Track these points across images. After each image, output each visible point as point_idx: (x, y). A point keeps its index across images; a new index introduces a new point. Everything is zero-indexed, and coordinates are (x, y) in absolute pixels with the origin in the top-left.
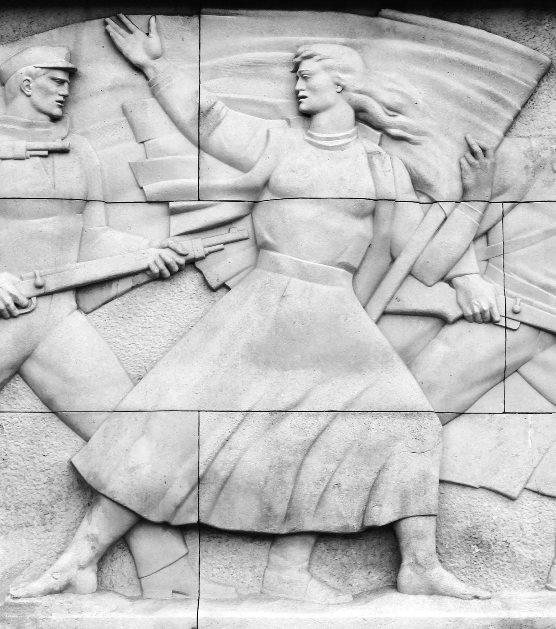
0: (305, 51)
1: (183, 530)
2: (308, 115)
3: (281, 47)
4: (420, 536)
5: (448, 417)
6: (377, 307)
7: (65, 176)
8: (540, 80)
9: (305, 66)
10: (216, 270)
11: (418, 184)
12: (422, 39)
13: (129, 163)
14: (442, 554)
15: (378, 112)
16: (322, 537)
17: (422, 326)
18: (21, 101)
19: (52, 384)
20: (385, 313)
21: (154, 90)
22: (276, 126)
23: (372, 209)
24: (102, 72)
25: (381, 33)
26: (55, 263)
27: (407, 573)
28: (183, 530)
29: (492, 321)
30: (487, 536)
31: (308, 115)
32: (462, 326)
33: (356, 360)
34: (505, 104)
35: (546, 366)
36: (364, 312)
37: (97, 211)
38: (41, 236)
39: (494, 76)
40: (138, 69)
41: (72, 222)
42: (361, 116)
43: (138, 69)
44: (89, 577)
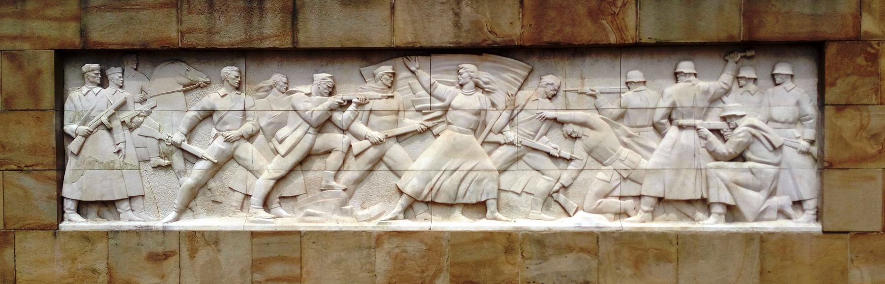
0: (461, 66)
1: (427, 203)
2: (462, 86)
3: (453, 65)
4: (492, 204)
5: (502, 171)
7: (393, 104)
8: (529, 73)
9: (461, 71)
11: (493, 105)
12: (495, 62)
14: (498, 209)
16: (466, 205)
19: (390, 163)
21: (417, 78)
23: (478, 113)
24: (403, 74)
25: (483, 61)
26: (631, 83)
27: (488, 214)
28: (427, 203)
30: (512, 204)
32: (505, 146)
33: (473, 155)
34: (82, 207)
37: (401, 113)
38: (387, 121)
40: (413, 72)
41: (394, 117)
42: (477, 86)
43: (413, 72)
44: (402, 216)
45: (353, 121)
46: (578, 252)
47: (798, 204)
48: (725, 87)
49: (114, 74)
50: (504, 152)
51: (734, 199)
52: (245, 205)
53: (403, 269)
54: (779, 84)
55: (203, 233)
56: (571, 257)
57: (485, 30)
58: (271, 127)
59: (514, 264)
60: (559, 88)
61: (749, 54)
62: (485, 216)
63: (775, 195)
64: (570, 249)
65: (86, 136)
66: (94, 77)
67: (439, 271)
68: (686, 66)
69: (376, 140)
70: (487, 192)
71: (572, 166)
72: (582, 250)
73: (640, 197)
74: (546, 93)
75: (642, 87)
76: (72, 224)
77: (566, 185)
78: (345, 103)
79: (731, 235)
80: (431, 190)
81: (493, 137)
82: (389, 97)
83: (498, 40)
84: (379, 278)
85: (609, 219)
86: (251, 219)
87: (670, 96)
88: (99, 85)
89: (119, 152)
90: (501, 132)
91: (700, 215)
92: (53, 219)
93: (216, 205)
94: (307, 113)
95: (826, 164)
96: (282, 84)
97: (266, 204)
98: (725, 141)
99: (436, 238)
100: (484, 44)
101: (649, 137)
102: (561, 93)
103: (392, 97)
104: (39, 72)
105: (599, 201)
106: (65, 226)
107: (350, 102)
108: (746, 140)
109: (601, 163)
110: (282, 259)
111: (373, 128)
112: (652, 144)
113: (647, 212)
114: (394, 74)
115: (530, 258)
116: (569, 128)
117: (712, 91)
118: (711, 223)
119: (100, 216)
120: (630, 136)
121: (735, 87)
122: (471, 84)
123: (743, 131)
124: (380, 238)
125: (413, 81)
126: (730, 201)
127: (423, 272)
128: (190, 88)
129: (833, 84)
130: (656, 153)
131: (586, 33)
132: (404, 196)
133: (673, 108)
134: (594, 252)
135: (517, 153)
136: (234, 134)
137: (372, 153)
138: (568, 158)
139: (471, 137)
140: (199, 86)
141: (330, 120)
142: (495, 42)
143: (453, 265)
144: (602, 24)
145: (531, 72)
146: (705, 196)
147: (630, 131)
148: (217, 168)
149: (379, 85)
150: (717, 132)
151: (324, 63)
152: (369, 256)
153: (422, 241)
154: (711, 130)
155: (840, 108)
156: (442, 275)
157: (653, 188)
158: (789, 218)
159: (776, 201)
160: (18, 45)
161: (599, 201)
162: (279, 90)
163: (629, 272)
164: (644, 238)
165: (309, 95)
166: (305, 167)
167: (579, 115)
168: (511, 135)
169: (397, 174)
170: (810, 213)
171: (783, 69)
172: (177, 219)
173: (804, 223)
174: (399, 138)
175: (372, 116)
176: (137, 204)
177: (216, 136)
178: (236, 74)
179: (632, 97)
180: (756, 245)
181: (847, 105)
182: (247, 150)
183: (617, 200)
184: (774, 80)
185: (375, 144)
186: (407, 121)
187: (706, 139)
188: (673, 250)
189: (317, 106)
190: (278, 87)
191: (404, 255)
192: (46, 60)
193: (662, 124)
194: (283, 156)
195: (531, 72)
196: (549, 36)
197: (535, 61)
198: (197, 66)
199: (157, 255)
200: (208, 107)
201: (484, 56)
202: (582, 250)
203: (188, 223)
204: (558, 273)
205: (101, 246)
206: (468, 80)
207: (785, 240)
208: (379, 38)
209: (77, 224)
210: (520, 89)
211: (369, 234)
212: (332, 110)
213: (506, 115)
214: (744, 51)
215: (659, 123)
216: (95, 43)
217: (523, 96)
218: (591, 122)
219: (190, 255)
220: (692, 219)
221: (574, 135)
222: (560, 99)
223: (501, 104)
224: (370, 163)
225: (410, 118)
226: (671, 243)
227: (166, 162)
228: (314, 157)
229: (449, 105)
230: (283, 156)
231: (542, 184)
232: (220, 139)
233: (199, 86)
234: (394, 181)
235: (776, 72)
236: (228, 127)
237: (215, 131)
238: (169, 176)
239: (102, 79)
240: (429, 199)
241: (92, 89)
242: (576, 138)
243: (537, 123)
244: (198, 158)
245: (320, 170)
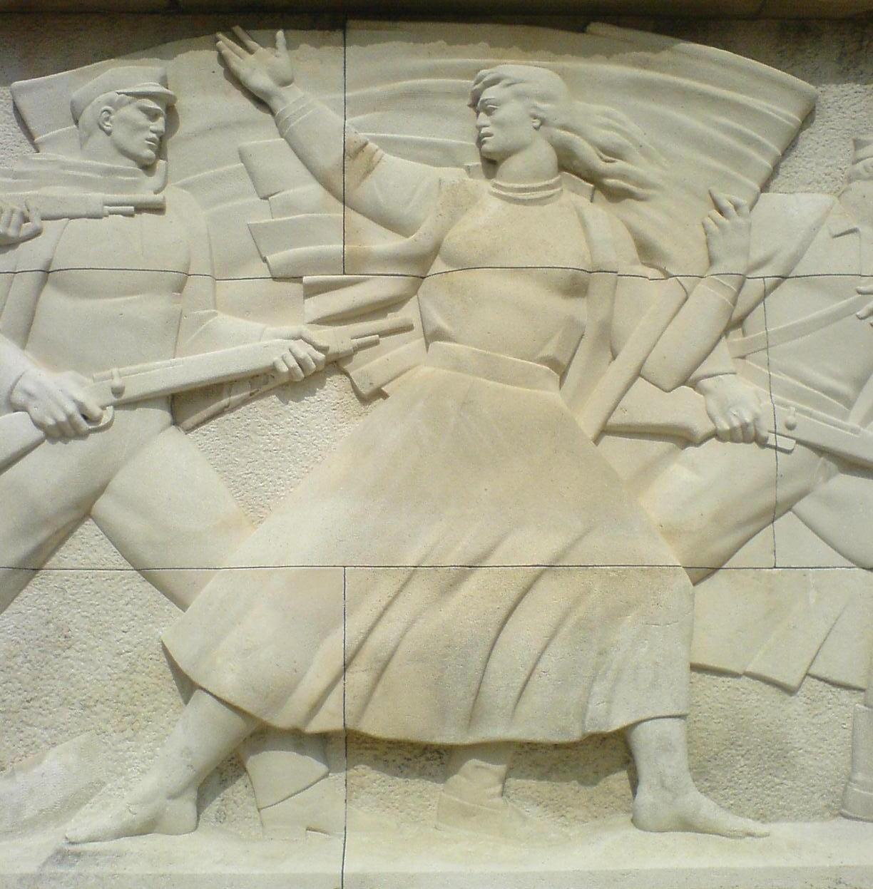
2: (491, 164)
4: (666, 747)
5: (702, 573)
11: (646, 251)
17: (657, 447)
23: (576, 287)
27: (646, 795)
40: (261, 101)
41: (152, 307)
42: (567, 162)
44: (186, 807)
50: (692, 484)
63: (617, 355)
82: (141, 208)
90: (689, 380)
103: (158, 209)
111: (54, 356)
122: (542, 154)
125: (262, 139)
132: (202, 703)
135: (776, 481)
169: (161, 579)
174: (184, 404)
185: (61, 432)
186: (226, 322)
206: (525, 131)
210: (765, 187)
213: (708, 301)
220: (780, 375)
223: (684, 248)
225: (245, 310)
229: (436, 250)
240: (326, 721)
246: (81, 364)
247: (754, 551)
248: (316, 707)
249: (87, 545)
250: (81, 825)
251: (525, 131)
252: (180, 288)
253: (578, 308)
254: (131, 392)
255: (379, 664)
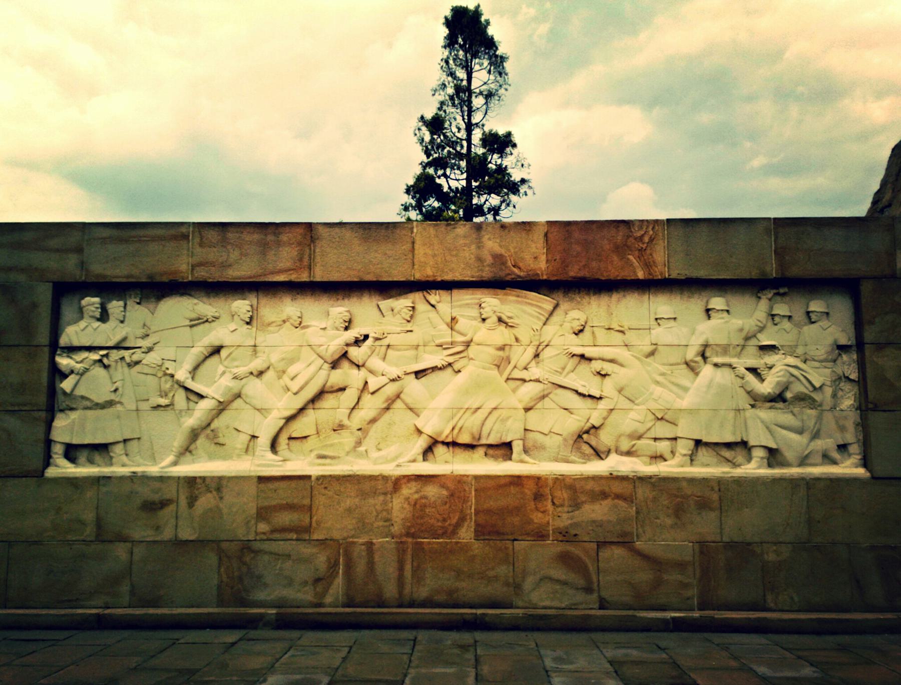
0: (483, 300)
2: (484, 320)
3: (476, 299)
5: (527, 410)
6: (505, 376)
7: (412, 339)
10: (457, 366)
11: (517, 340)
12: (518, 296)
13: (257, 437)
15: (504, 318)
16: (490, 446)
17: (519, 383)
18: (398, 316)
19: (409, 400)
20: (508, 379)
22: (475, 323)
23: (502, 348)
25: (506, 294)
29: (539, 381)
31: (484, 320)
32: (531, 383)
34: (72, 452)
35: (556, 394)
36: (463, 372)
37: (421, 348)
39: (540, 307)
40: (433, 306)
41: (412, 353)
42: (500, 320)
43: (433, 306)
44: (421, 457)
45: (369, 356)
46: (613, 499)
47: (843, 448)
48: (760, 324)
49: (115, 306)
50: (529, 391)
51: (777, 444)
52: (250, 449)
53: (422, 518)
54: (813, 323)
55: (204, 479)
56: (607, 503)
57: (509, 264)
58: (282, 363)
59: (543, 512)
60: (586, 323)
61: (782, 291)
62: (510, 459)
64: (604, 495)
65: (82, 374)
66: (94, 311)
67: (462, 519)
68: (717, 302)
69: (394, 376)
70: (511, 432)
71: (603, 405)
72: (618, 497)
73: (675, 439)
74: (572, 328)
75: (672, 323)
76: (60, 470)
77: (597, 425)
78: (362, 338)
79: (776, 481)
80: (453, 429)
81: (517, 374)
83: (522, 274)
84: (396, 528)
85: (645, 463)
86: (257, 462)
87: (702, 333)
88: (98, 320)
89: (116, 390)
90: (526, 368)
91: (740, 459)
92: (37, 463)
93: (218, 448)
94: (322, 348)
95: (871, 406)
96: (296, 318)
97: (274, 446)
98: (762, 380)
99: (459, 482)
100: (509, 278)
101: (683, 376)
102: (587, 329)
104: (34, 306)
105: (634, 442)
106: (51, 472)
107: (366, 337)
108: (785, 379)
109: (633, 402)
110: (290, 507)
112: (686, 382)
113: (685, 455)
114: (413, 308)
115: (562, 505)
116: (597, 365)
117: (747, 328)
118: (754, 468)
119: (91, 462)
120: (663, 374)
121: (770, 324)
122: (495, 319)
123: (781, 370)
124: (397, 483)
125: (433, 314)
126: (774, 446)
127: (444, 520)
128: (198, 321)
129: (872, 323)
130: (691, 391)
131: (613, 270)
133: (706, 346)
134: (628, 499)
135: (544, 390)
136: (242, 370)
137: (391, 389)
138: (598, 396)
139: (495, 372)
140: (207, 321)
141: (345, 355)
142: (519, 277)
143: (477, 512)
144: (628, 259)
145: (556, 307)
146: (745, 439)
147: (663, 369)
148: (222, 407)
149: (398, 320)
150: (753, 371)
151: (340, 297)
152: (385, 503)
153: (443, 486)
154: (748, 369)
155: (880, 346)
156: (466, 524)
157: (688, 429)
158: (834, 462)
159: (820, 444)
160: (13, 277)
161: (634, 442)
162: (292, 325)
163: (669, 521)
164: (684, 484)
165: (324, 329)
166: (317, 405)
167: (608, 352)
168: (535, 371)
170: (856, 458)
171: (816, 306)
172: (175, 463)
173: (849, 468)
174: (419, 374)
175: (390, 351)
176: (133, 445)
177: (224, 373)
178: (249, 308)
179: (663, 334)
180: (802, 492)
181: (889, 344)
182: (254, 388)
183: (652, 442)
184: (810, 318)
186: (426, 356)
187: (743, 378)
188: (715, 496)
189: (336, 341)
190: (291, 321)
191: (423, 501)
192: (44, 294)
193: (696, 362)
194: (295, 394)
195: (556, 307)
196: (574, 272)
197: (559, 295)
198: (205, 299)
199: (153, 503)
200: (217, 343)
201: (508, 291)
202: (618, 497)
203: (187, 469)
204: (594, 522)
205: (90, 494)
206: (491, 314)
207: (835, 482)
208: (398, 274)
209: (64, 470)
210: (544, 324)
211: (385, 478)
212: (347, 345)
213: (531, 351)
214: (777, 289)
215: (692, 361)
216: (98, 276)
217: (550, 330)
218: (620, 360)
219: (189, 503)
221: (603, 373)
222: (586, 336)
223: (525, 340)
224: (387, 400)
225: (431, 353)
226: (712, 489)
227: (163, 401)
228: (326, 395)
230: (295, 394)
231: (572, 424)
232: (228, 376)
233: (207, 321)
234: (411, 420)
235: (810, 309)
236: (236, 363)
237: (221, 368)
238: (168, 415)
239: (101, 314)
240: (449, 440)
241: (90, 323)
242: (604, 376)
243: (565, 359)
244: (201, 397)
245: (334, 409)
246: (397, 365)
247: (539, 405)
248: (447, 437)
249: (398, 404)
250: (401, 460)
251: (491, 314)
252: (417, 349)
253: (501, 353)
254: (408, 371)
255: (78, 273)
